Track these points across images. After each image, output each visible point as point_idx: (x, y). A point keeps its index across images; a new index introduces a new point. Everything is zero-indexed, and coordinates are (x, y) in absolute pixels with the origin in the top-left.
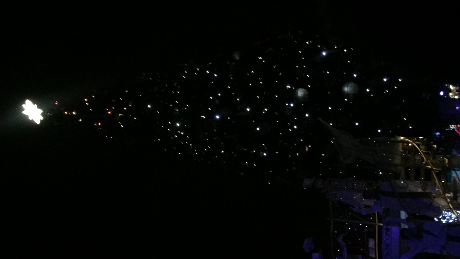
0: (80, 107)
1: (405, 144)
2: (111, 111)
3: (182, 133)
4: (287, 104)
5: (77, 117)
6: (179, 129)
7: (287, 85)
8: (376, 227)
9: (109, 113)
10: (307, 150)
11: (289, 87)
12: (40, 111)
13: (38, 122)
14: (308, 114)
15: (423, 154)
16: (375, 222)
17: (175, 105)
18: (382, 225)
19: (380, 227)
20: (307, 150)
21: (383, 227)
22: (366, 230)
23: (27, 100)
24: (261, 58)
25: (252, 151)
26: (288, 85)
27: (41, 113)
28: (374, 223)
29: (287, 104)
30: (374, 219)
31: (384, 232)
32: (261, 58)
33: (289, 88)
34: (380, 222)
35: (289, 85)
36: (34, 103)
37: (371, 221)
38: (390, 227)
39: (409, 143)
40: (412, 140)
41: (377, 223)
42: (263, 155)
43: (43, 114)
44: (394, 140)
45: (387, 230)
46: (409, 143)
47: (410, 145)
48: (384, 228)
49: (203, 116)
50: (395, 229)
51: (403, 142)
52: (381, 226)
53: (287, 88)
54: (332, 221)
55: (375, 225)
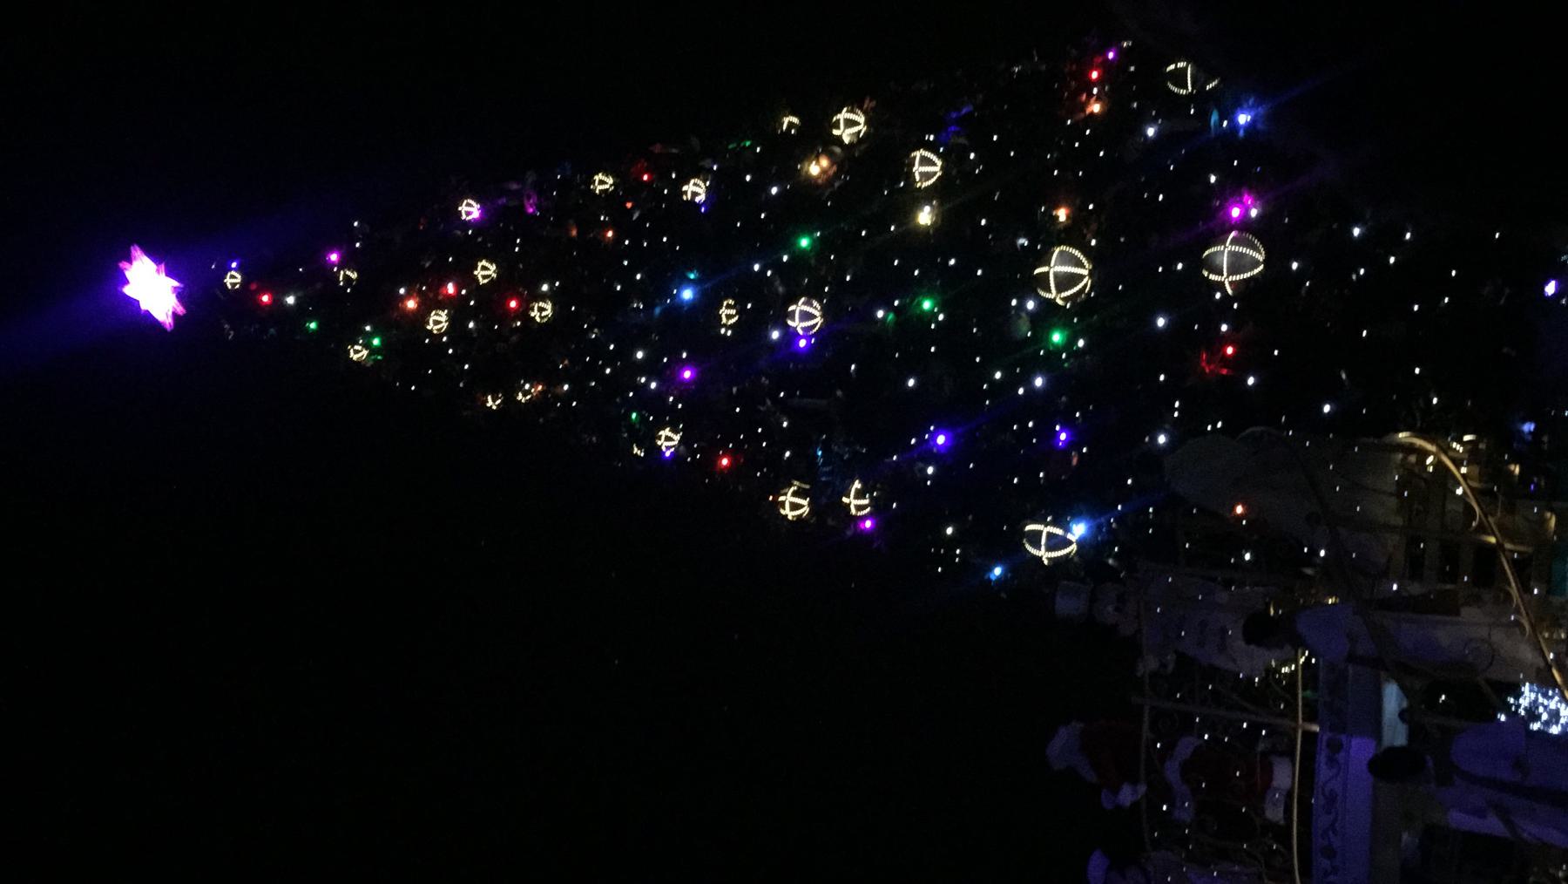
3: (1177, 404)
4: (703, 210)
5: (301, 312)
6: (642, 367)
11: (1023, 241)
15: (1474, 495)
16: (1295, 719)
18: (1316, 728)
21: (1320, 736)
22: (1261, 747)
28: (1293, 725)
29: (703, 210)
30: (1292, 705)
31: (1322, 758)
34: (1311, 717)
37: (1282, 714)
38: (1343, 738)
40: (1439, 446)
41: (1300, 721)
43: (180, 295)
44: (1267, 784)
45: (1335, 747)
49: (340, 282)
50: (1360, 750)
51: (1409, 449)
52: (1315, 734)
55: (1295, 730)
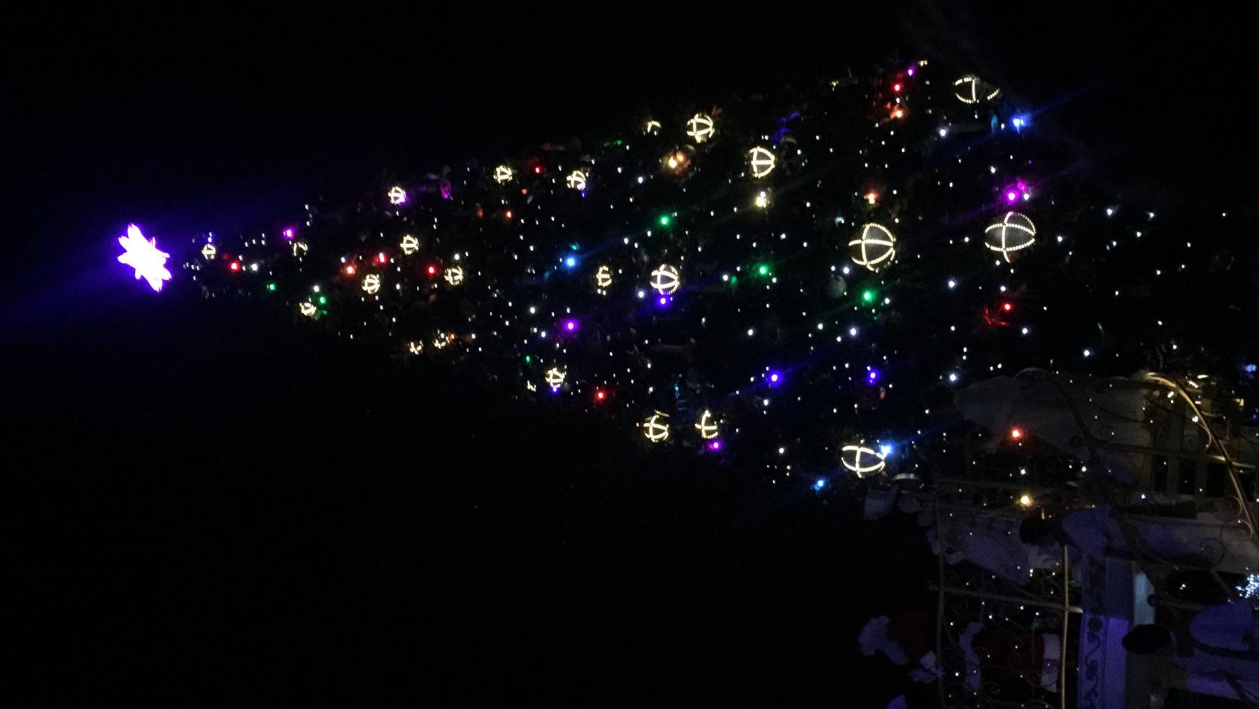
0: (277, 254)
1: (1157, 393)
2: (356, 266)
5: (263, 276)
6: (534, 320)
7: (836, 216)
8: (1064, 616)
9: (853, 332)
10: (883, 395)
12: (163, 257)
13: (157, 285)
14: (428, 271)
16: (1063, 603)
17: (526, 258)
19: (1074, 616)
20: (883, 395)
23: (133, 226)
24: (434, 226)
25: (399, 294)
26: (840, 216)
27: (164, 261)
28: (1060, 606)
31: (1086, 630)
32: (434, 226)
33: (840, 223)
34: (1075, 602)
35: (842, 216)
36: (148, 237)
37: (1052, 599)
38: (1102, 618)
39: (1168, 389)
40: (1177, 383)
42: (760, 406)
45: (1096, 625)
46: (1168, 389)
47: (1171, 395)
48: (1088, 617)
51: (1156, 385)
53: (577, 244)
54: (942, 595)
